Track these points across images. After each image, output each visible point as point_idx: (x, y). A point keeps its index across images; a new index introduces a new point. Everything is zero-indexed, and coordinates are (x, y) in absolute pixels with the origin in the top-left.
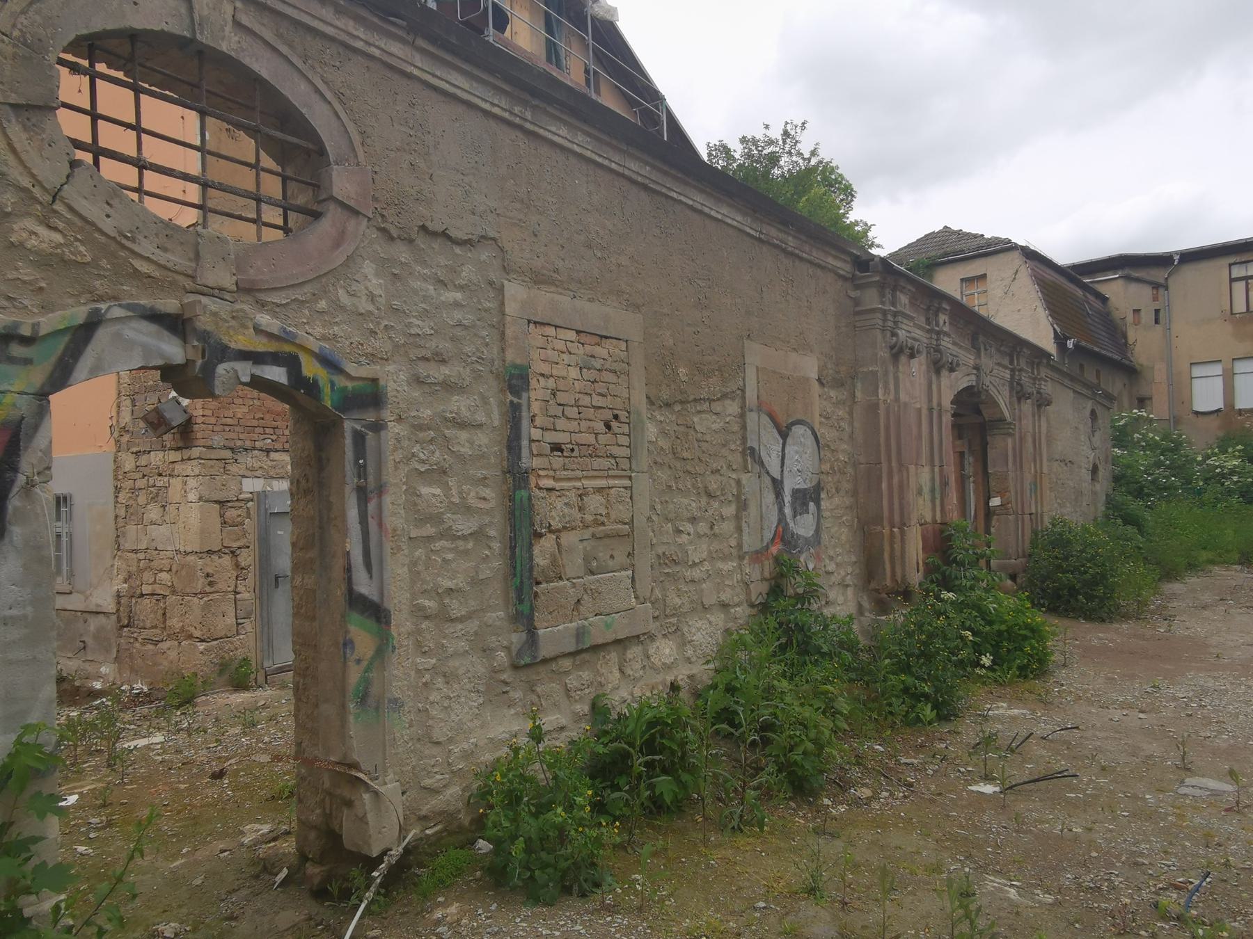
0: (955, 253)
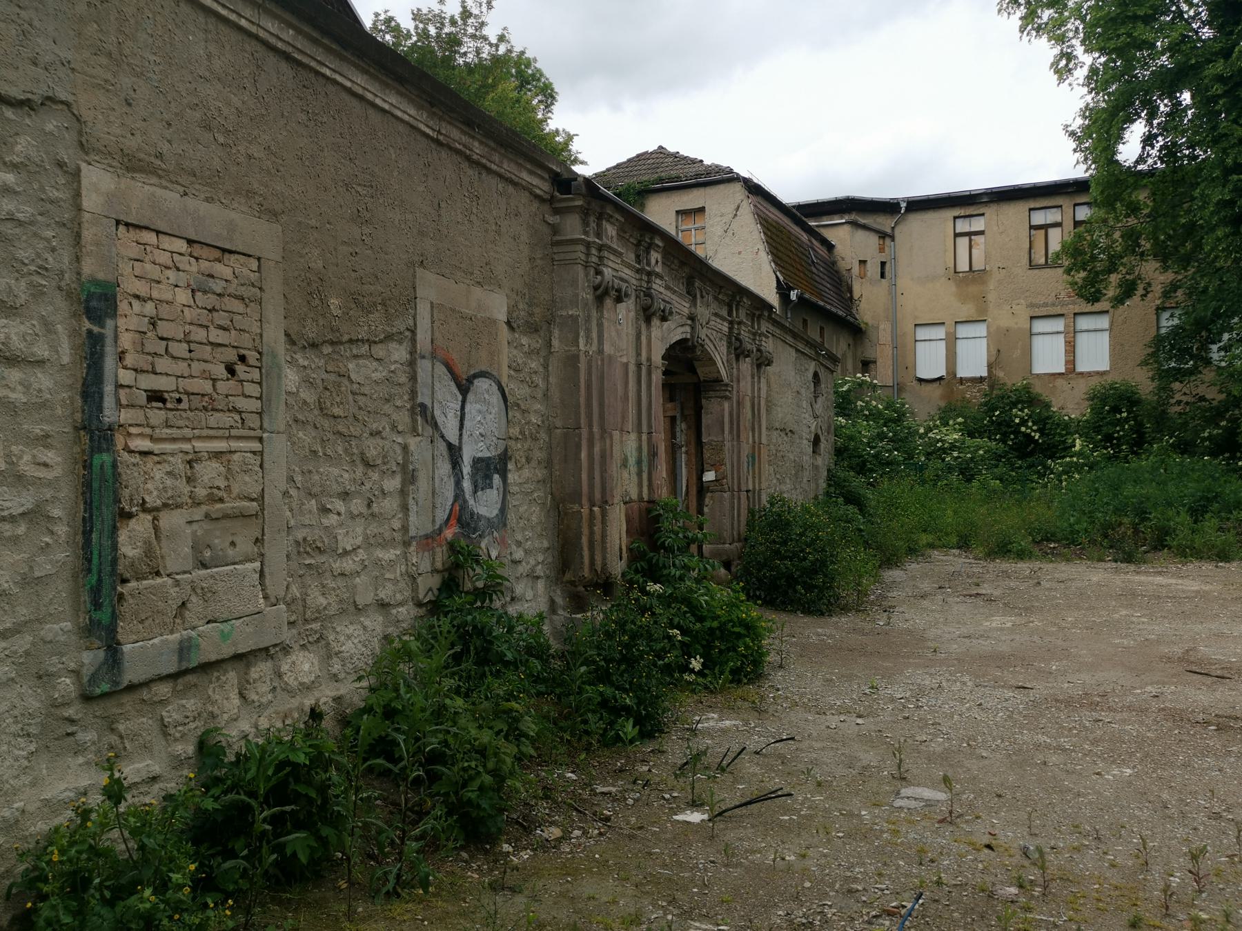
0: (671, 180)
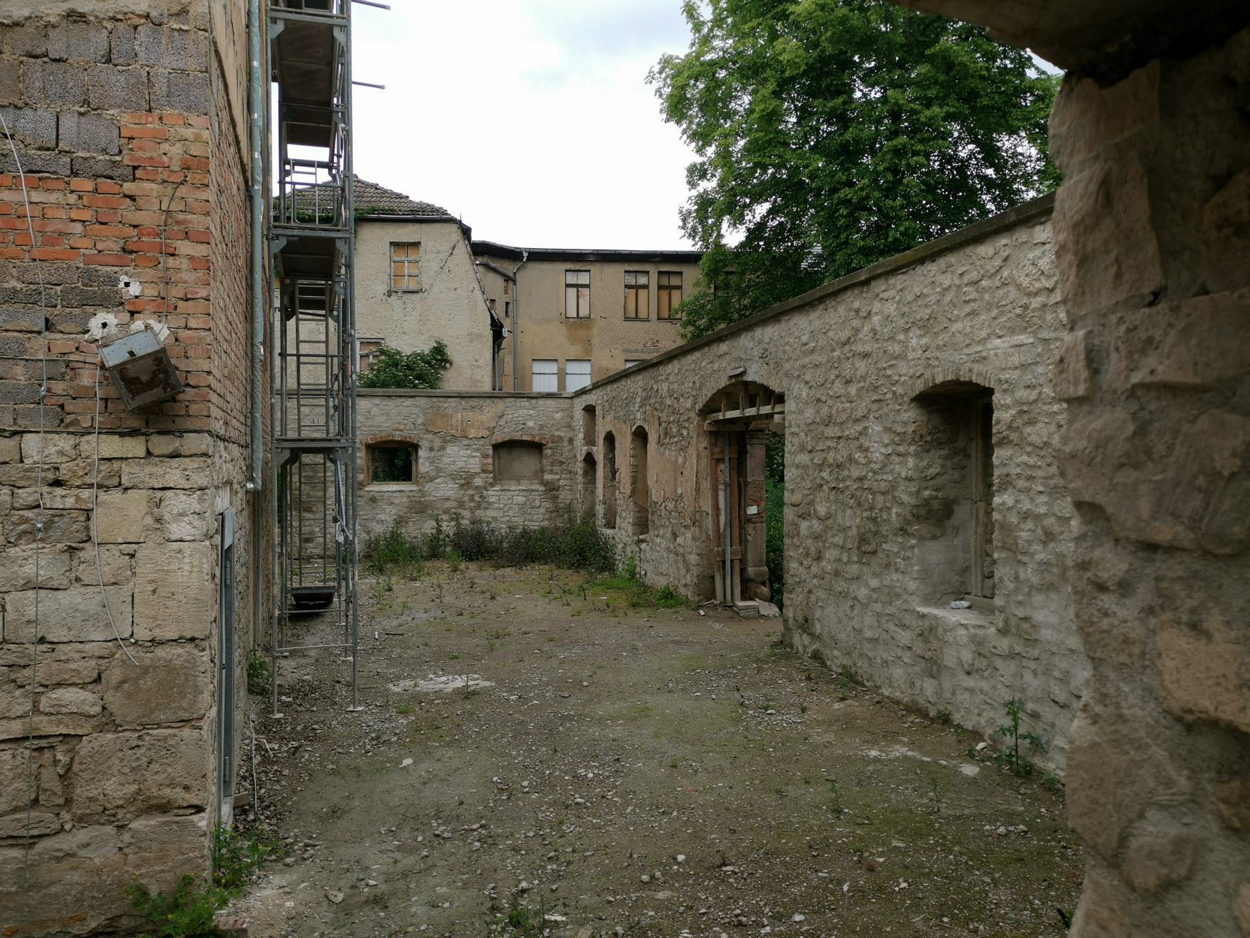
0: (384, 211)
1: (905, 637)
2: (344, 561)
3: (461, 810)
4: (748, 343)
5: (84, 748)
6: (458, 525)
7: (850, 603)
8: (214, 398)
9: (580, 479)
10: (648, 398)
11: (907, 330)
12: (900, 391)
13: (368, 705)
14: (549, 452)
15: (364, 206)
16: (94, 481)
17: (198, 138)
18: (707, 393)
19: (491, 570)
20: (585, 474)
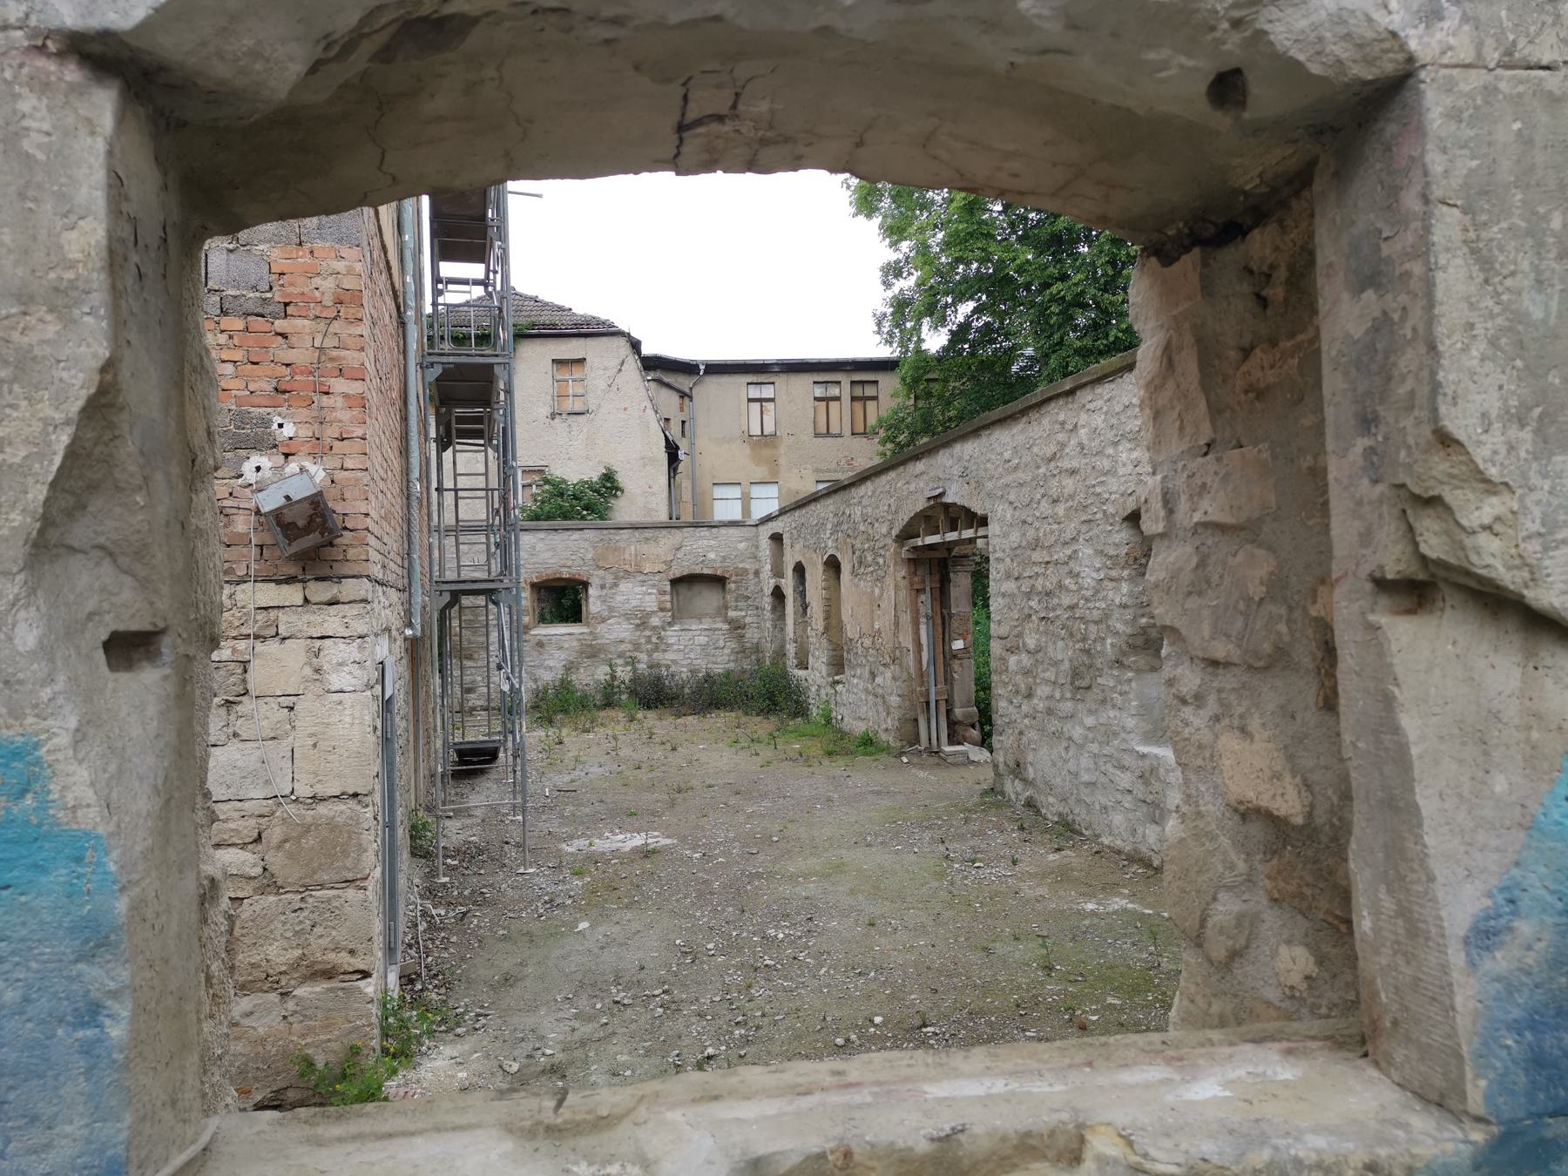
1: (1125, 780)
2: (510, 713)
3: (642, 975)
4: (945, 461)
5: (246, 911)
6: (635, 670)
7: (1065, 744)
8: (372, 540)
9: (768, 615)
10: (839, 524)
11: (1116, 444)
12: (1111, 510)
13: (539, 866)
14: (733, 586)
15: (523, 321)
16: (250, 632)
17: (350, 272)
18: (904, 518)
19: (671, 719)
20: (774, 609)
